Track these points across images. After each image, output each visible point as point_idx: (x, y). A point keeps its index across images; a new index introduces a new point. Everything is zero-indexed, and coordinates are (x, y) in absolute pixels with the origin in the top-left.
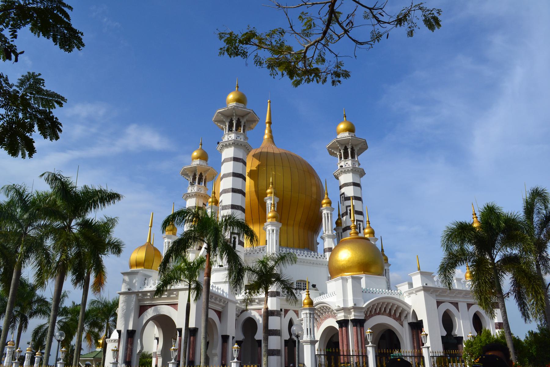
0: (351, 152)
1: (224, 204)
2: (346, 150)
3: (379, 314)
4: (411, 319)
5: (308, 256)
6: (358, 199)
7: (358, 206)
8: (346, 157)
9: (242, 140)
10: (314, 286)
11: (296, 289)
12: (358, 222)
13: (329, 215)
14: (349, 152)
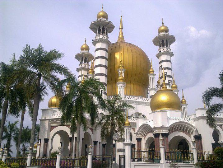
0: (166, 43)
1: (96, 73)
2: (163, 41)
3: (177, 131)
4: (195, 134)
5: (133, 99)
6: (170, 69)
7: (169, 73)
8: (163, 46)
9: (105, 38)
10: (143, 116)
11: (133, 117)
12: (169, 82)
13: (153, 78)
14: (101, 30)
